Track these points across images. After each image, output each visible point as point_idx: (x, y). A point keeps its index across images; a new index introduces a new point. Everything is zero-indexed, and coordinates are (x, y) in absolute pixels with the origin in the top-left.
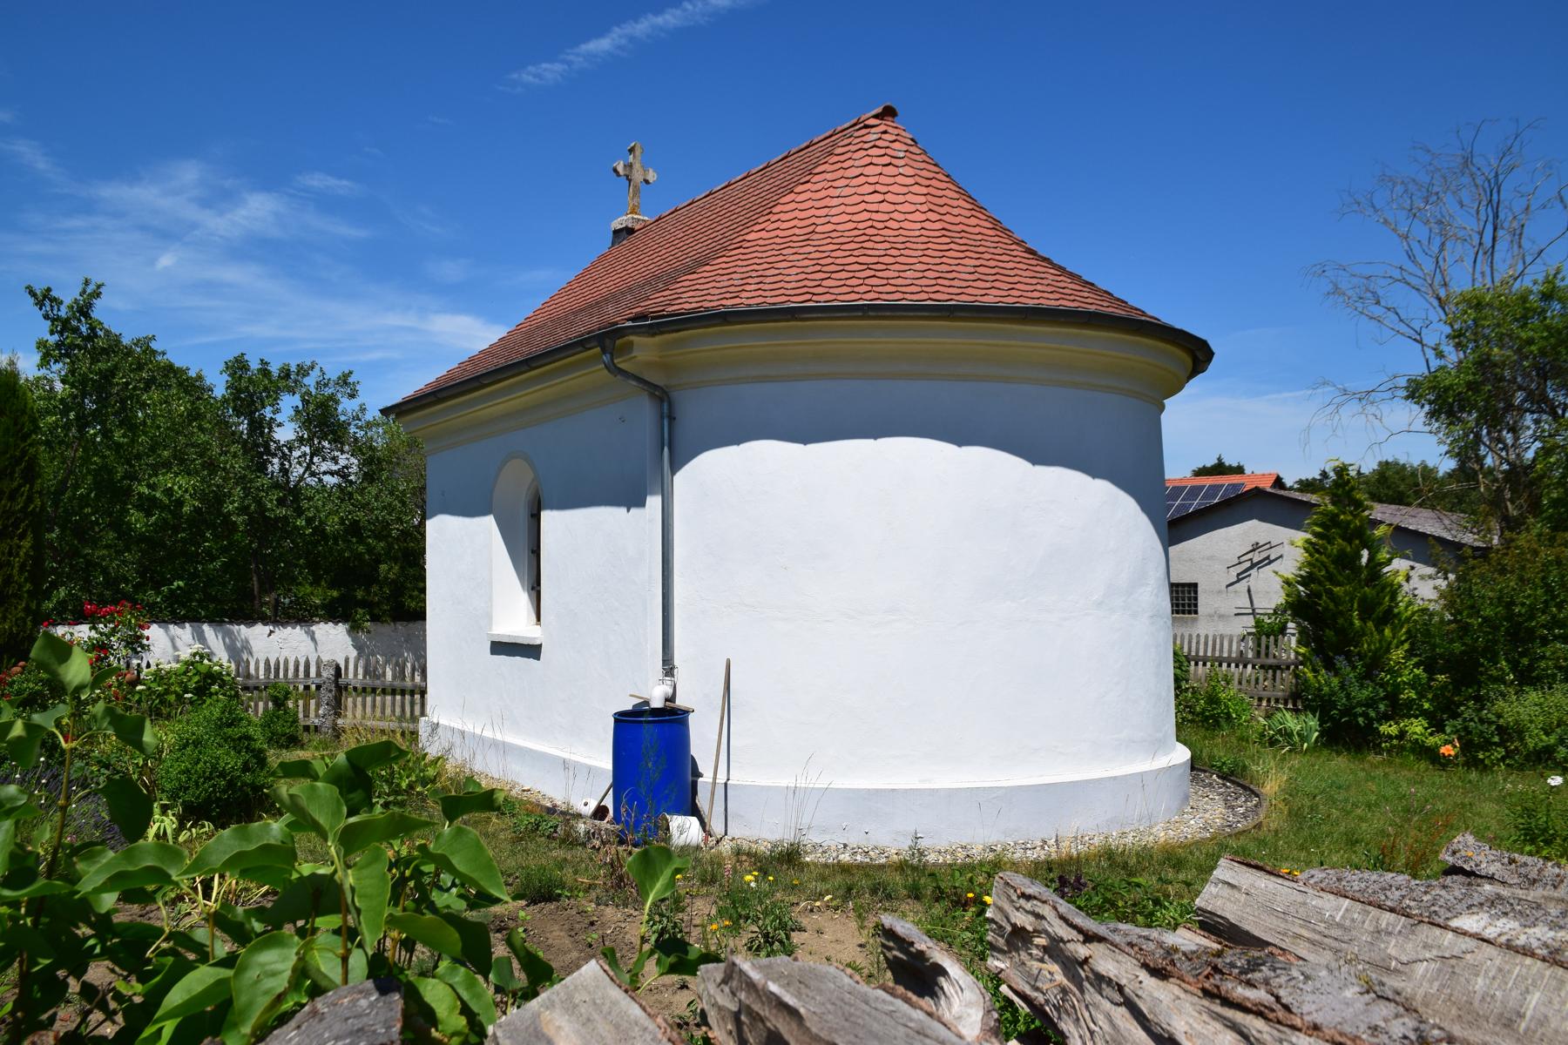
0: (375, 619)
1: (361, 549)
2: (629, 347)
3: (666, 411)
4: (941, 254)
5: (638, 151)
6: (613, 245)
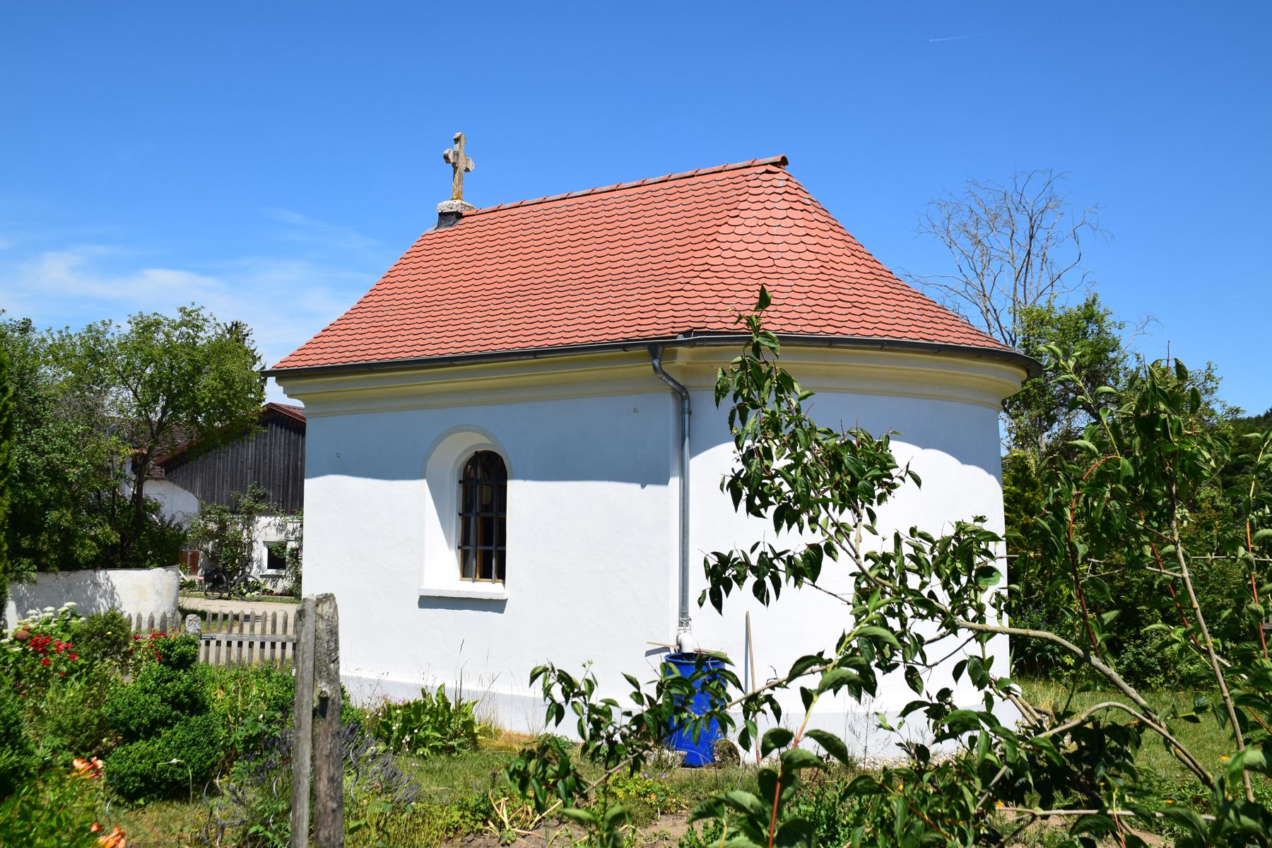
0: (42, 569)
1: (30, 495)
2: (673, 355)
3: (686, 407)
4: (810, 283)
5: (463, 140)
6: (438, 227)
